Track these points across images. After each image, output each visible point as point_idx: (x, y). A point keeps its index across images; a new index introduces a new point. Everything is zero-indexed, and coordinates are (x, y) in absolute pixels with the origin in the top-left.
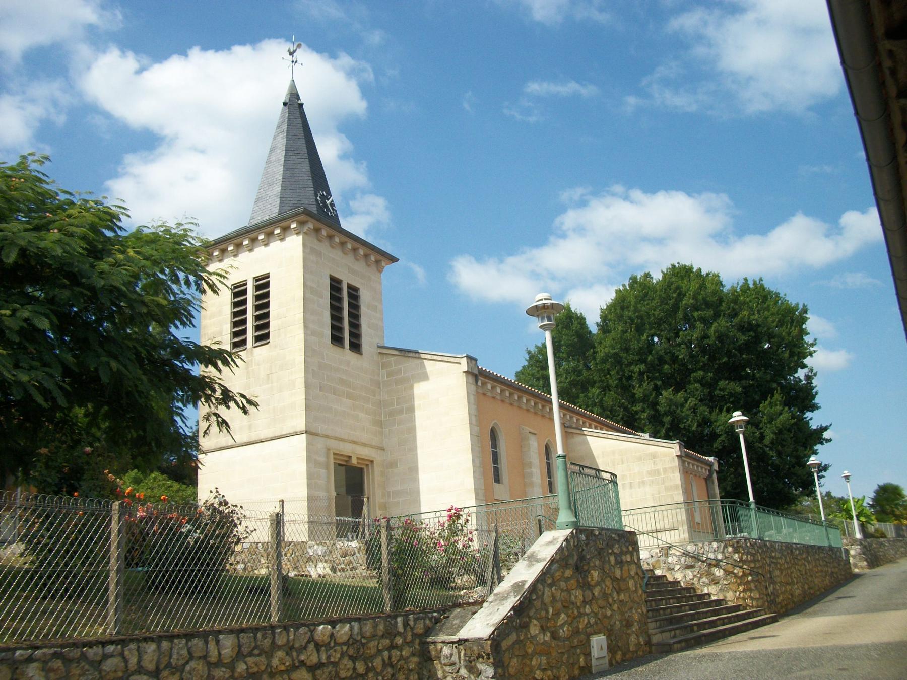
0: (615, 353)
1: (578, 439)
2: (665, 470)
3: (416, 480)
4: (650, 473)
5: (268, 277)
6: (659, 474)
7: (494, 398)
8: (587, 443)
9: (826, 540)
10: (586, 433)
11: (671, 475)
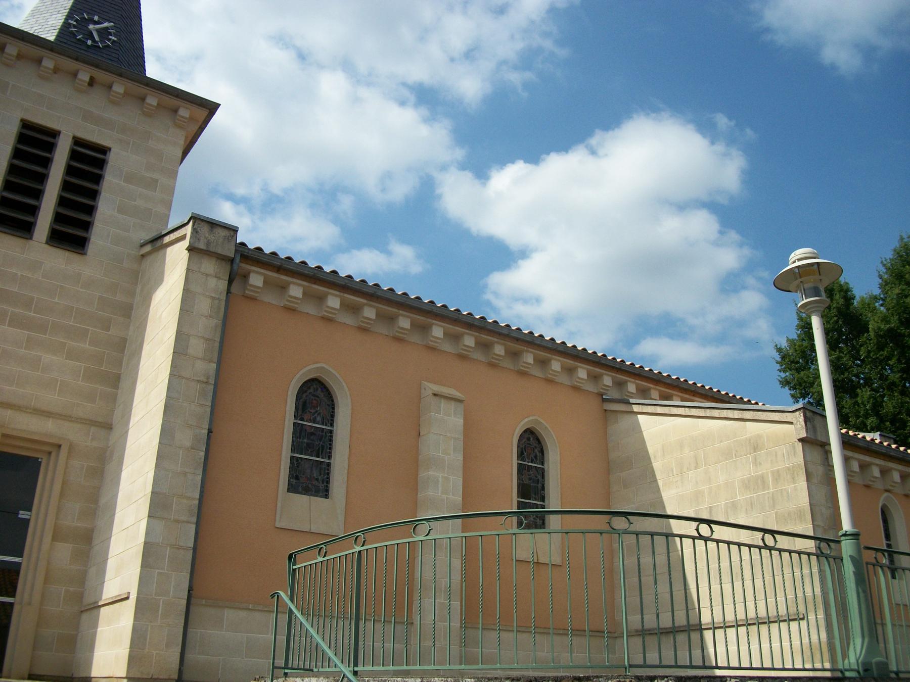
0: (890, 330)
1: (624, 422)
2: (777, 476)
3: (72, 6)
4: (747, 485)
5: (57, 238)
6: (765, 486)
7: (867, 486)
8: (637, 429)
9: (884, 542)
10: (636, 408)
11: (790, 487)
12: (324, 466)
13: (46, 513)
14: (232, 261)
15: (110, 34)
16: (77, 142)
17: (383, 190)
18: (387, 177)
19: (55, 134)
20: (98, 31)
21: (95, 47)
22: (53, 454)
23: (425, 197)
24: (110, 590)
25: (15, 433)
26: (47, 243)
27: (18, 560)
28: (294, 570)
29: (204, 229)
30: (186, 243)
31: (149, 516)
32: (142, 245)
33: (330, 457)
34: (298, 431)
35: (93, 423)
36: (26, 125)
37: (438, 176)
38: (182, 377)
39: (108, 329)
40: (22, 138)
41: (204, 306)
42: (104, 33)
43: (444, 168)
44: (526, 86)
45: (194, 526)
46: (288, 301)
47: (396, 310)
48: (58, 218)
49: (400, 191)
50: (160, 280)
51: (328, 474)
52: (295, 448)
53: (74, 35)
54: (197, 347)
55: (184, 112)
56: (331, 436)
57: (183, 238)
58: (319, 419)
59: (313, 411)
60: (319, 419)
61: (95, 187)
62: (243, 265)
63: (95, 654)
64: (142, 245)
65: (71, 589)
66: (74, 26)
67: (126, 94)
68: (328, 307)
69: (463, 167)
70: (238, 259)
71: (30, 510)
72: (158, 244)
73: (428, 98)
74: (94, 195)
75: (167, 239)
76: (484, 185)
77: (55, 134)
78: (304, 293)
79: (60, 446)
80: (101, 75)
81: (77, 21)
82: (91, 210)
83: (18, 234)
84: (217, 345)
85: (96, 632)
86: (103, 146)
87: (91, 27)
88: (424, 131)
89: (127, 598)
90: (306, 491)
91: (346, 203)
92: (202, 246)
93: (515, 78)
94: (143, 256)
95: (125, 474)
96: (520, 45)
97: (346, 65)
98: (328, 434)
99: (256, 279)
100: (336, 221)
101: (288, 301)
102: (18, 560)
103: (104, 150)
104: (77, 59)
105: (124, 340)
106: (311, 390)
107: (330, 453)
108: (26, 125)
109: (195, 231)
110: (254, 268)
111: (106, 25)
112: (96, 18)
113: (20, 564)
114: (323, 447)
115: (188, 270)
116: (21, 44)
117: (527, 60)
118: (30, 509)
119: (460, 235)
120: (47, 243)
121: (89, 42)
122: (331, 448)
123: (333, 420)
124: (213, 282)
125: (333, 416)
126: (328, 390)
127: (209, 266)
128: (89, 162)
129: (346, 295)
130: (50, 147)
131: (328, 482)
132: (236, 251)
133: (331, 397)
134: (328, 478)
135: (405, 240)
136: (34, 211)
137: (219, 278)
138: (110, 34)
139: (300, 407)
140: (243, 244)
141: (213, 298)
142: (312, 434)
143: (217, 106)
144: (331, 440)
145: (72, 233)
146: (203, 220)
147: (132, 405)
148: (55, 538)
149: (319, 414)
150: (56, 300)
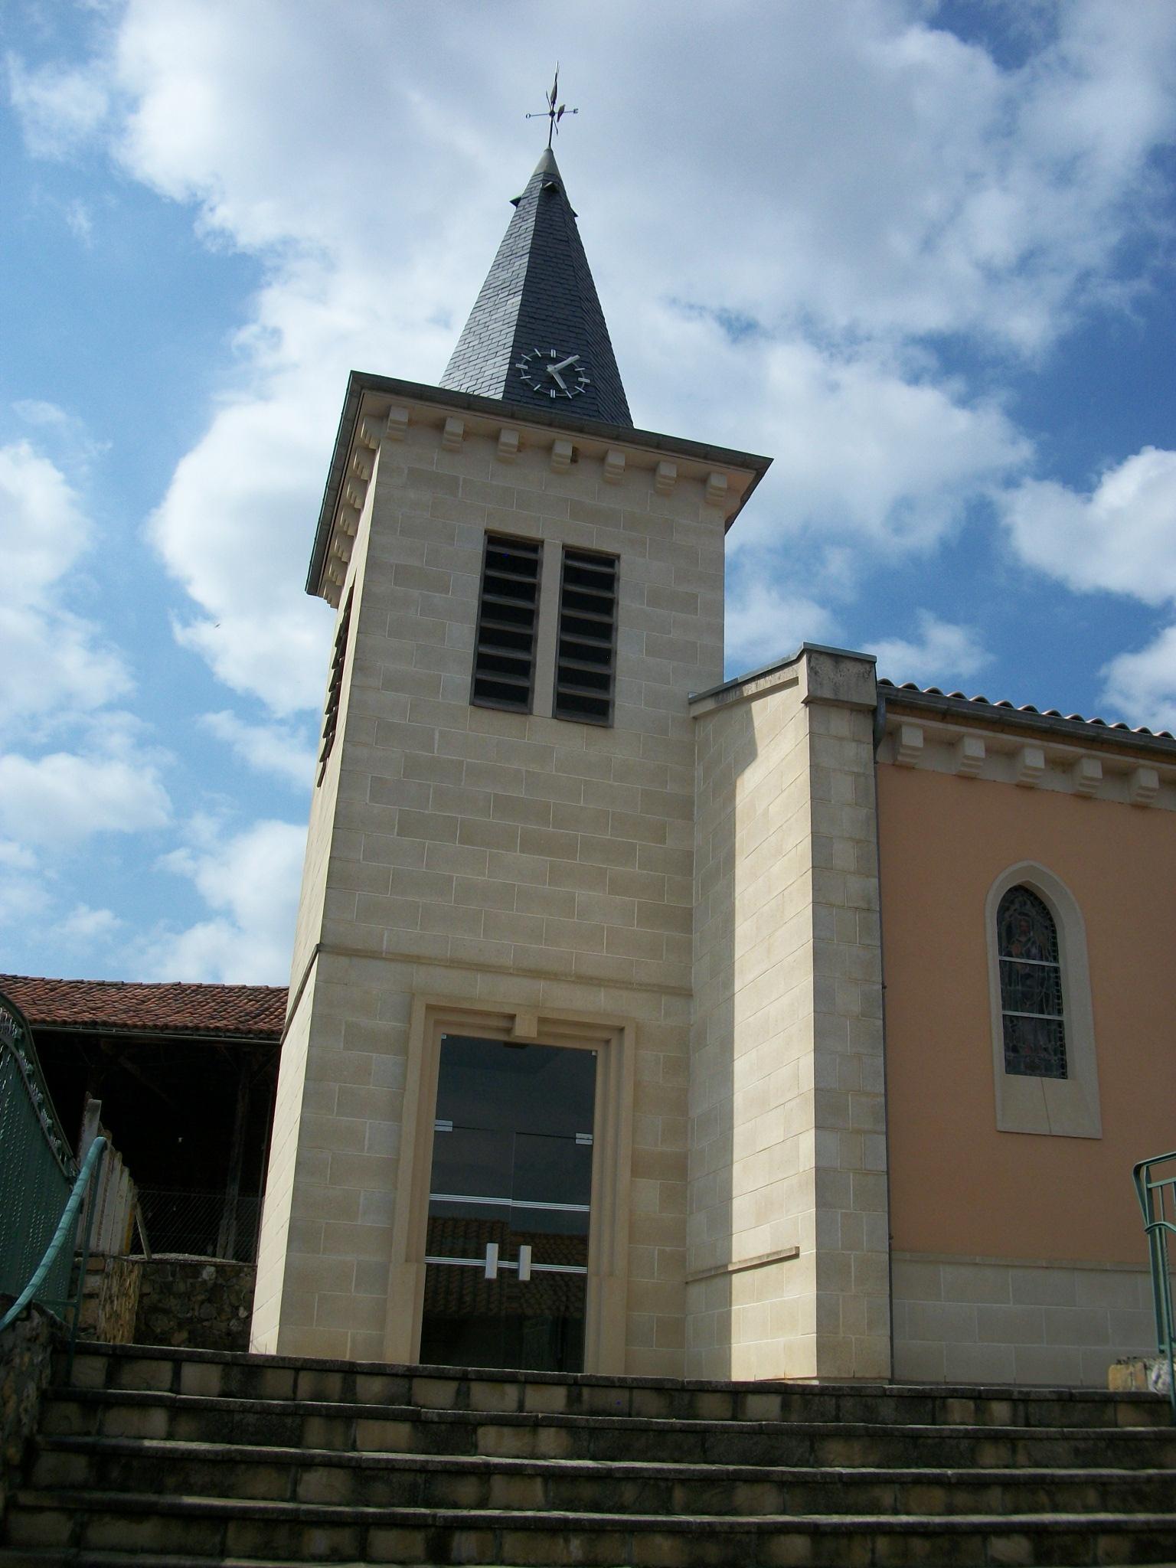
5: (568, 707)
12: (1053, 1027)
13: (618, 1132)
14: (874, 712)
15: (579, 375)
16: (570, 553)
17: (899, 530)
18: (902, 508)
19: (535, 546)
20: (561, 373)
21: (562, 399)
22: (614, 1044)
23: (978, 537)
24: (748, 1241)
25: (555, 1016)
26: (555, 717)
27: (584, 1208)
28: (1149, 1190)
29: (826, 666)
30: (802, 690)
31: (818, 1127)
32: (693, 702)
33: (1060, 1012)
34: (1008, 973)
35: (660, 989)
36: (493, 539)
37: (999, 496)
38: (832, 905)
39: (663, 840)
40: (491, 560)
41: (844, 788)
42: (569, 373)
43: (1011, 481)
44: (1140, 304)
45: (884, 1137)
46: (964, 764)
47: (1131, 760)
48: (564, 675)
49: (928, 532)
50: (747, 754)
51: (1062, 1039)
52: (1008, 1001)
53: (524, 383)
54: (845, 856)
55: (718, 481)
56: (1058, 977)
57: (794, 682)
58: (1034, 951)
59: (1023, 939)
60: (1034, 951)
61: (605, 619)
62: (889, 716)
63: (735, 1346)
64: (693, 702)
65: (668, 1249)
66: (526, 373)
67: (629, 466)
68: (1026, 767)
69: (1043, 474)
70: (883, 709)
71: (591, 1131)
72: (732, 696)
73: (955, 360)
74: (606, 631)
75: (751, 689)
76: (1090, 500)
77: (535, 546)
78: (988, 750)
79: (622, 1030)
80: (591, 444)
81: (527, 363)
82: (606, 656)
83: (511, 708)
84: (873, 847)
85: (729, 1313)
86: (607, 554)
87: (550, 368)
88: (961, 420)
89: (796, 1256)
90: (1032, 1069)
91: (838, 564)
92: (827, 693)
93: (1115, 295)
94: (695, 718)
95: (742, 1064)
96: (1113, 238)
97: (809, 327)
98: (1052, 975)
99: (912, 735)
100: (824, 602)
101: (964, 764)
102: (584, 1208)
103: (610, 560)
104: (550, 425)
105: (689, 855)
106: (1017, 906)
107: (1059, 1004)
108: (493, 539)
109: (812, 671)
110: (905, 719)
111: (570, 360)
112: (553, 353)
113: (587, 1215)
114: (1047, 995)
115: (812, 734)
116: (468, 415)
117: (1128, 261)
118: (590, 1130)
119: (1052, 593)
120: (555, 717)
121: (553, 393)
122: (1059, 997)
123: (1056, 951)
124: (851, 750)
125: (1055, 944)
126: (1041, 903)
127: (842, 724)
128: (592, 581)
129: (1052, 745)
130: (532, 567)
131: (1063, 1053)
132: (879, 695)
133: (1048, 913)
134: (1063, 1046)
135: (948, 618)
136: (526, 669)
137: (859, 741)
138: (579, 375)
139: (1004, 934)
140: (886, 682)
141: (857, 775)
142: (1028, 976)
143: (769, 461)
144: (1058, 984)
145: (586, 697)
146: (821, 653)
147: (732, 956)
148: (635, 1173)
149: (1034, 943)
150: (582, 804)
